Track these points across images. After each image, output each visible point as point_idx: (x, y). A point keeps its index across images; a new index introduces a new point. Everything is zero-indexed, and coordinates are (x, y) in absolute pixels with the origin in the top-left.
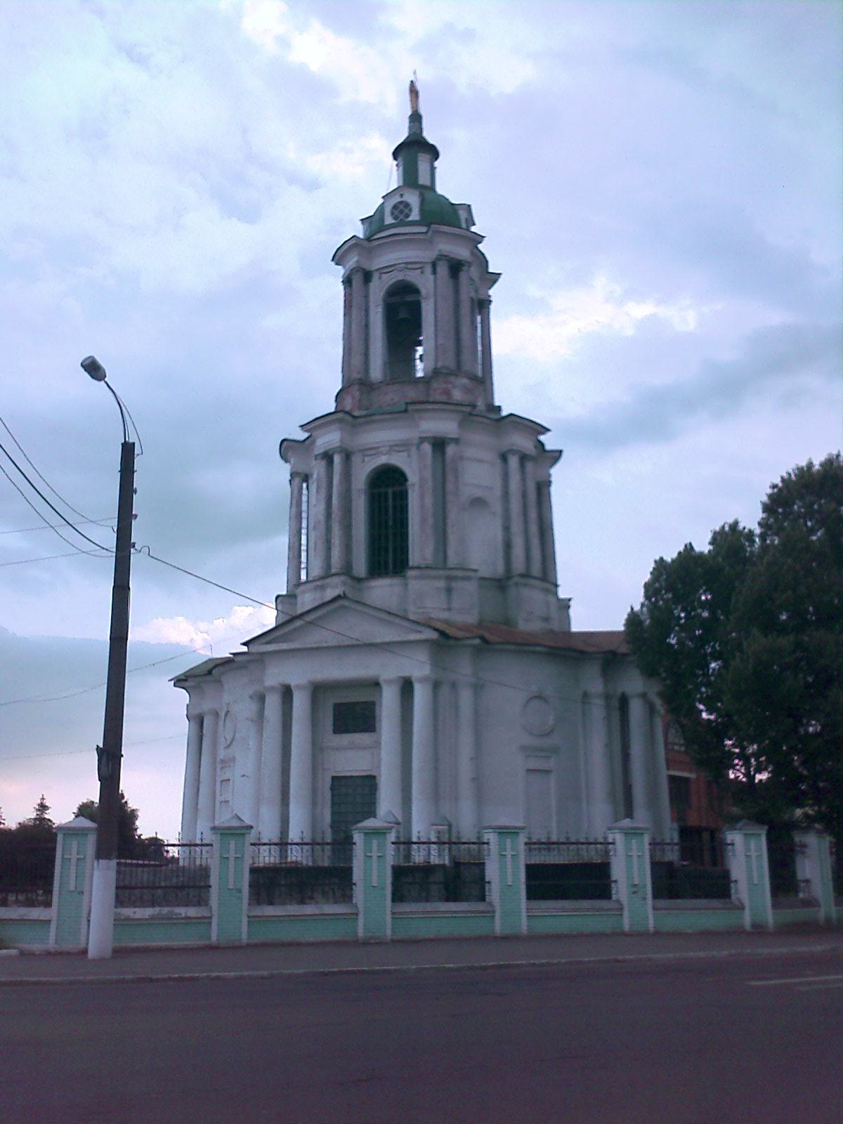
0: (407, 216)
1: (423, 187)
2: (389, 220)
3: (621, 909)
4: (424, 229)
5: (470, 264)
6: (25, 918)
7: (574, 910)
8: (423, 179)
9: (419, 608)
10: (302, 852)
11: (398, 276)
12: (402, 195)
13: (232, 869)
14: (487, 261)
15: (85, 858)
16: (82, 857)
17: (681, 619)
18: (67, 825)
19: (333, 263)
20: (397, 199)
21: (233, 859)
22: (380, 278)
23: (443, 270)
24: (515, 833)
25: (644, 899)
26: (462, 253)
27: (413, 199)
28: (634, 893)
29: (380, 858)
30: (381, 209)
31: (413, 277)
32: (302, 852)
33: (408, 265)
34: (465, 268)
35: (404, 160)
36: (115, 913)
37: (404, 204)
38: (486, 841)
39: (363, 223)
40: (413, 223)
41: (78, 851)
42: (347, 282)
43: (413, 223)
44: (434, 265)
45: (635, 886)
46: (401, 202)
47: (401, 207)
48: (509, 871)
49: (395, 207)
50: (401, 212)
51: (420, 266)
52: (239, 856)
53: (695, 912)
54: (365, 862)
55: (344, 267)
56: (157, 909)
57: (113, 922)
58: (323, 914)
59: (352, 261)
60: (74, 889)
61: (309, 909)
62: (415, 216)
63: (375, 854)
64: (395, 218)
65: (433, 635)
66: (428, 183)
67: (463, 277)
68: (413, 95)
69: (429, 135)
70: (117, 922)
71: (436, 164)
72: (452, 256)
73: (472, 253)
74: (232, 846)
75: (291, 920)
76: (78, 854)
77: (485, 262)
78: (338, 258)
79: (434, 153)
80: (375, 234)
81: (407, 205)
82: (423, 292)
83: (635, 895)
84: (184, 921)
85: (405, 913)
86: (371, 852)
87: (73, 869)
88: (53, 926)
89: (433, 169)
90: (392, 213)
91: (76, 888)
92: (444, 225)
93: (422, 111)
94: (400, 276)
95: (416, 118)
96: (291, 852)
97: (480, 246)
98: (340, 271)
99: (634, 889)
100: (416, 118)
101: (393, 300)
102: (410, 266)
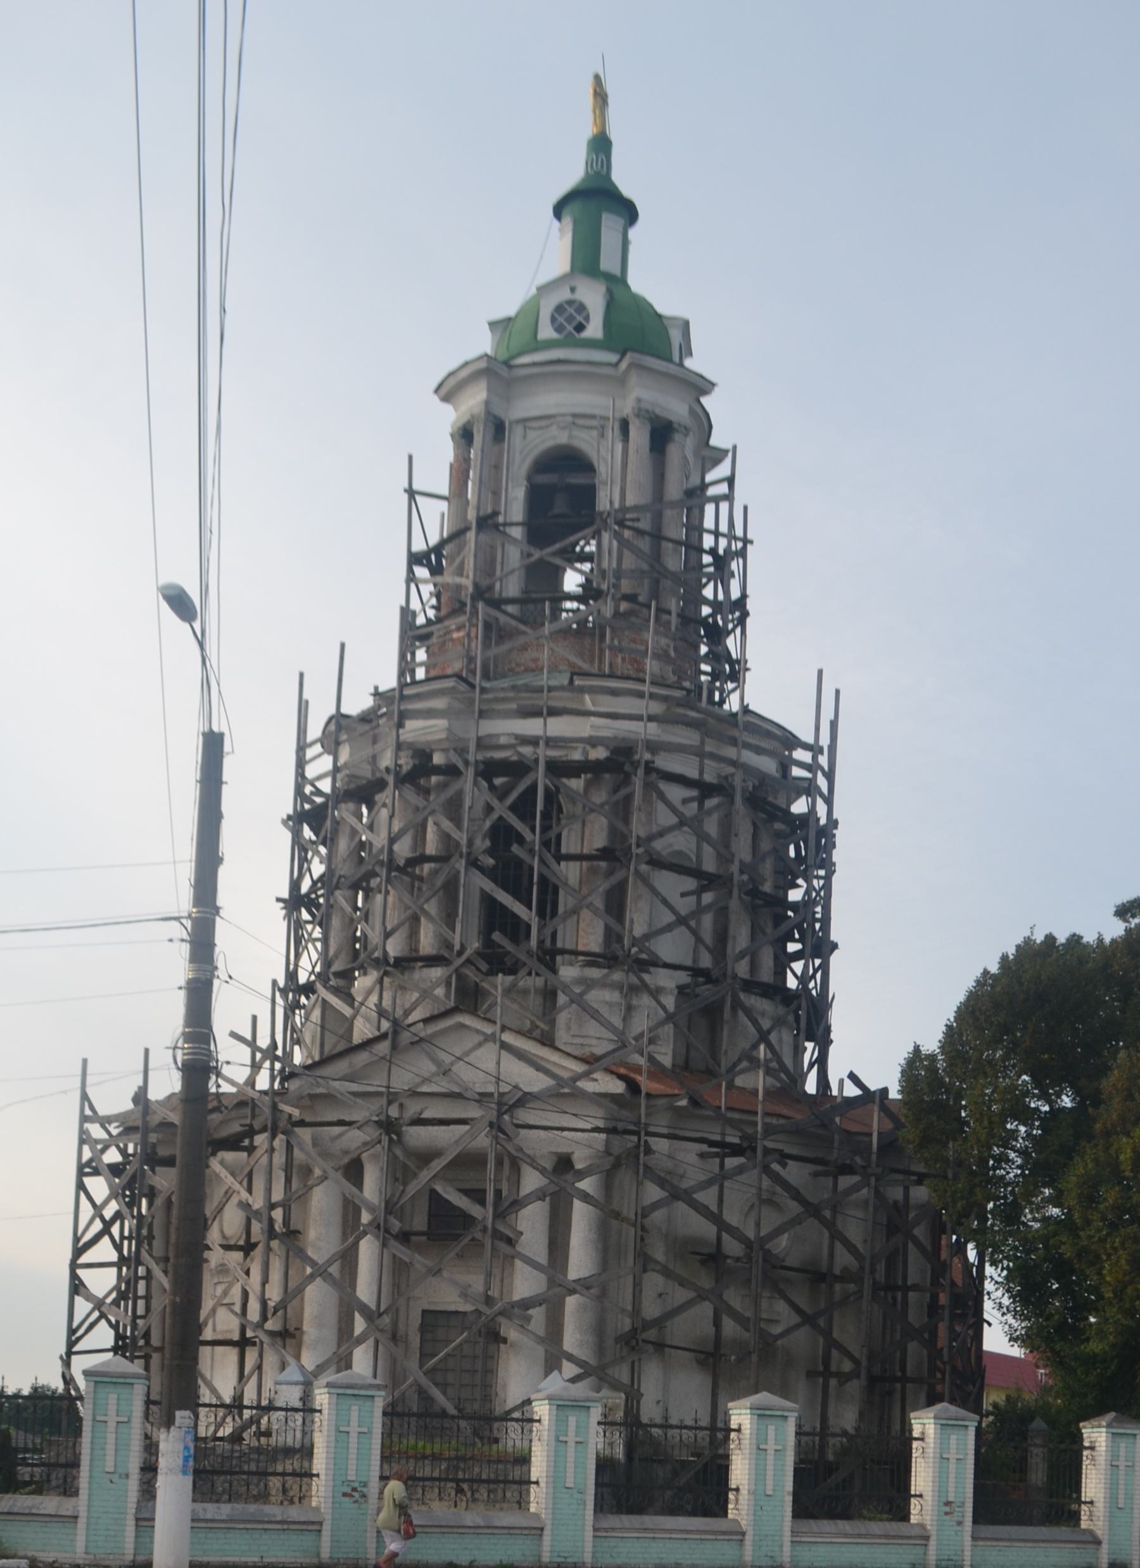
0: (580, 328)
1: (609, 278)
2: (546, 332)
3: (927, 1538)
4: (613, 358)
5: (687, 430)
6: (34, 1511)
7: (859, 1536)
8: (608, 262)
9: (573, 1036)
10: (523, 1432)
11: (557, 437)
12: (573, 290)
13: (353, 1451)
14: (710, 427)
15: (128, 1422)
16: (126, 1419)
17: (1055, 1091)
18: (94, 1369)
19: (436, 398)
20: (564, 295)
21: (773, 1452)
22: (524, 437)
23: (639, 436)
24: (782, 1416)
25: (960, 1523)
26: (676, 408)
27: (593, 297)
28: (946, 1514)
29: (579, 1445)
30: (531, 310)
31: (585, 442)
32: (523, 1432)
33: (577, 419)
34: (677, 437)
35: (576, 223)
36: (193, 1511)
37: (575, 306)
38: (537, 1418)
39: (491, 330)
40: (591, 344)
41: (118, 1411)
42: (464, 435)
43: (591, 344)
44: (625, 425)
45: (948, 1503)
46: (570, 303)
47: (571, 310)
48: (770, 1473)
49: (560, 309)
50: (570, 319)
51: (599, 424)
52: (365, 1430)
53: (1054, 1545)
54: (556, 1451)
55: (456, 409)
56: (239, 1507)
57: (189, 1524)
58: (488, 1527)
59: (475, 398)
60: (112, 1470)
61: (471, 1518)
62: (594, 329)
63: (571, 1438)
64: (559, 329)
65: (617, 1087)
66: (617, 271)
67: (673, 452)
68: (599, 100)
69: (624, 179)
70: (196, 1525)
71: (633, 233)
72: (658, 411)
73: (692, 412)
74: (354, 1414)
75: (509, 1534)
76: (117, 1415)
77: (707, 427)
78: (448, 391)
79: (629, 212)
80: (520, 354)
81: (581, 308)
82: (602, 469)
83: (947, 1517)
84: (279, 1526)
85: (613, 1529)
86: (567, 1436)
87: (111, 1438)
88: (82, 1523)
89: (625, 243)
90: (553, 319)
91: (115, 1466)
92: (653, 355)
93: (614, 135)
94: (562, 438)
95: (601, 145)
96: (409, 1427)
97: (705, 400)
98: (448, 417)
99: (947, 1509)
100: (601, 145)
101: (543, 479)
102: (581, 422)
